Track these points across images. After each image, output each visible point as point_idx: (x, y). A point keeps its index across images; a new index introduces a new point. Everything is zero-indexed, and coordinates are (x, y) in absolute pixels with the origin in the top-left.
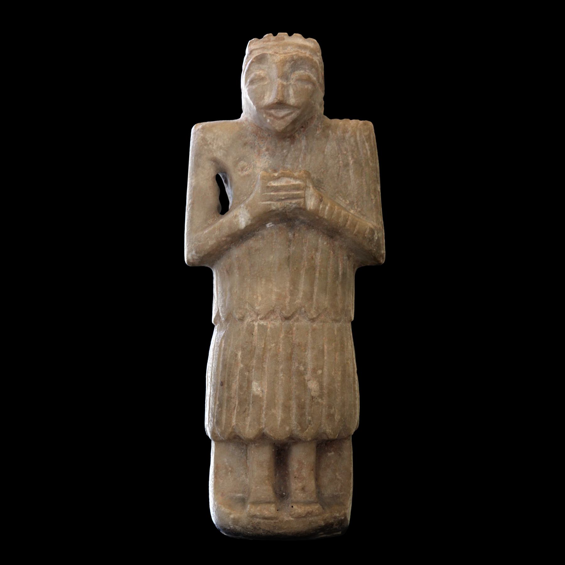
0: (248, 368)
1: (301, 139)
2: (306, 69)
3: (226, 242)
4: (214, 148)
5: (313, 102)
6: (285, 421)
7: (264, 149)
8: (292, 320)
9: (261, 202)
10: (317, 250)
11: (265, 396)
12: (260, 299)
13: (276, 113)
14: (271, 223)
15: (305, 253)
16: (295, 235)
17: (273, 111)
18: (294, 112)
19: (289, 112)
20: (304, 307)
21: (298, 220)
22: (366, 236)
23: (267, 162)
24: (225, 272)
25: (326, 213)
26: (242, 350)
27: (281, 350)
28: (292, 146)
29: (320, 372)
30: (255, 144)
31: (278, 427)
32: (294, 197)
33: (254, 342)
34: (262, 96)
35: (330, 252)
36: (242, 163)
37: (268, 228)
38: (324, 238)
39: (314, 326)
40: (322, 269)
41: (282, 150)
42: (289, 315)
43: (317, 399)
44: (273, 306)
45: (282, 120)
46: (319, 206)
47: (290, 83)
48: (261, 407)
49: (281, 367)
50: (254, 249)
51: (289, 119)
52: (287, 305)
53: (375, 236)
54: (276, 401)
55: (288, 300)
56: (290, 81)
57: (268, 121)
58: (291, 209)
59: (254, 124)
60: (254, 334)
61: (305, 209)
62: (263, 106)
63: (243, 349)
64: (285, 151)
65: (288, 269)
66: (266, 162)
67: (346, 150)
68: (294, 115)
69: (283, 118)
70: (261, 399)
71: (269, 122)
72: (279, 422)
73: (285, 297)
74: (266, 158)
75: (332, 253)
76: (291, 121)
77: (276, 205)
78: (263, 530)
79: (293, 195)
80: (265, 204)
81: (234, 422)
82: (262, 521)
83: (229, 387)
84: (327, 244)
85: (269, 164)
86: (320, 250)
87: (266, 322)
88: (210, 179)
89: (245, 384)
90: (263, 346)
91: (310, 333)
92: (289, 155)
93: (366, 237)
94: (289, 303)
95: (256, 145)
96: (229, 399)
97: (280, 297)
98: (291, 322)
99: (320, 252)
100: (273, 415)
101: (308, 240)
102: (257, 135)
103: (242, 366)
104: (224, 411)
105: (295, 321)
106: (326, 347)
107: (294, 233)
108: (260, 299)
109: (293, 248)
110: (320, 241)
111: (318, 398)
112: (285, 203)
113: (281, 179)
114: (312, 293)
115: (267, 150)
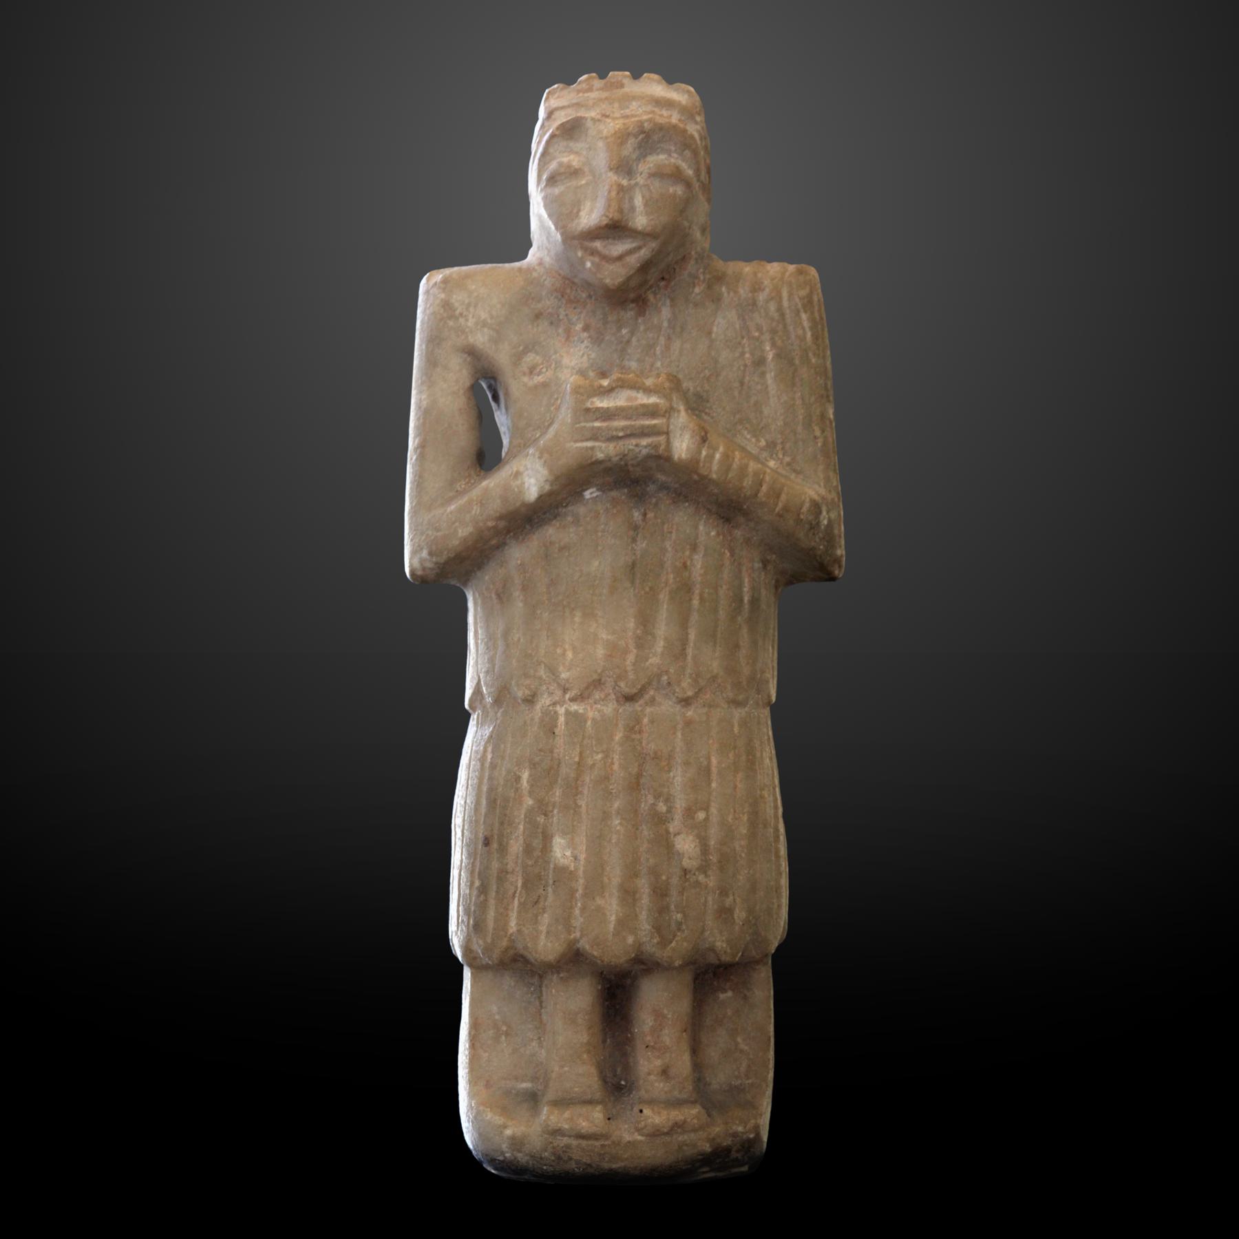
0: (543, 807)
1: (660, 304)
3: (496, 531)
5: (686, 224)
6: (626, 923)
7: (579, 327)
8: (641, 702)
10: (694, 548)
11: (582, 869)
12: (570, 655)
13: (605, 247)
14: (594, 489)
15: (669, 555)
16: (648, 516)
17: (598, 244)
18: (645, 246)
19: (634, 245)
20: (667, 672)
21: (654, 482)
22: (802, 517)
23: (586, 355)
24: (494, 596)
25: (715, 467)
26: (531, 768)
27: (616, 767)
28: (640, 321)
29: (701, 815)
30: (558, 316)
31: (610, 937)
32: (644, 433)
33: (558, 751)
34: (575, 211)
35: (724, 552)
36: (530, 358)
37: (588, 499)
38: (711, 521)
39: (688, 715)
40: (707, 590)
42: (634, 691)
43: (694, 874)
44: (599, 671)
45: (618, 264)
46: (700, 453)
47: (636, 182)
48: (572, 892)
49: (616, 805)
50: (557, 545)
52: (629, 668)
53: (822, 518)
54: (606, 879)
55: (631, 658)
57: (588, 265)
58: (639, 459)
59: (556, 272)
60: (556, 733)
61: (668, 459)
62: (576, 233)
63: (533, 765)
64: (624, 331)
66: (583, 355)
68: (644, 253)
69: (620, 258)
70: (572, 875)
71: (590, 269)
72: (612, 926)
73: (626, 652)
74: (583, 346)
75: (728, 554)
76: (639, 265)
77: (604, 451)
78: (577, 1162)
79: (643, 427)
80: (581, 448)
81: (513, 925)
82: (574, 1142)
83: (503, 850)
84: (718, 534)
85: (589, 359)
86: (701, 549)
87: (583, 707)
88: (462, 392)
89: (537, 843)
91: (681, 731)
93: (802, 520)
94: (634, 664)
95: (561, 317)
96: (503, 874)
97: (614, 651)
98: (637, 706)
99: (703, 552)
100: (599, 909)
102: (563, 296)
104: (492, 902)
105: (646, 704)
106: (714, 761)
107: (645, 510)
108: (570, 655)
109: (642, 545)
110: (701, 528)
111: (697, 873)
112: (624, 445)
113: (617, 393)
114: (684, 642)
115: (586, 328)
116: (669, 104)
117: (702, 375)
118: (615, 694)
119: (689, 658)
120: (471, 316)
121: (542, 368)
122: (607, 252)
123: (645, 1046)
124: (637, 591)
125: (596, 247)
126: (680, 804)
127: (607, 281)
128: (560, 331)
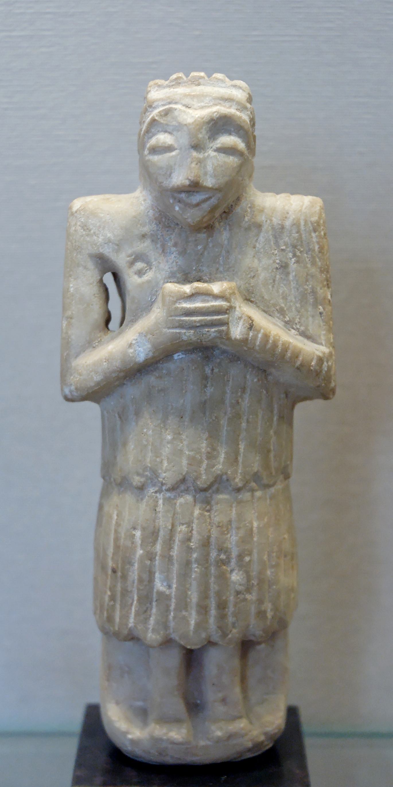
0: (151, 557)
1: (222, 229)
2: (231, 130)
3: (118, 378)
4: (100, 240)
5: (240, 178)
6: (200, 625)
7: (170, 244)
8: (210, 491)
9: (166, 329)
10: (244, 390)
11: (174, 593)
12: (165, 464)
13: (188, 197)
14: (181, 353)
15: (228, 396)
16: (214, 371)
17: (183, 195)
18: (214, 196)
19: (207, 196)
20: (226, 474)
21: (218, 349)
22: (312, 368)
23: (175, 262)
24: (117, 415)
25: (258, 343)
26: (141, 531)
27: (194, 532)
28: (209, 240)
29: (247, 559)
30: (157, 236)
31: (191, 633)
32: (212, 324)
33: (158, 521)
34: (168, 173)
35: (262, 391)
36: (139, 265)
37: (176, 360)
38: (254, 372)
39: (239, 497)
40: (251, 416)
41: (197, 245)
42: (205, 486)
43: (243, 594)
44: (184, 474)
45: (197, 208)
46: (249, 334)
47: (209, 154)
48: (168, 606)
49: (195, 555)
50: (157, 389)
51: (206, 206)
52: (203, 472)
53: (324, 366)
54: (189, 600)
55: (204, 465)
56: (208, 152)
57: (177, 208)
58: (209, 339)
59: (156, 206)
60: (157, 510)
61: (229, 339)
62: (169, 188)
63: (144, 529)
64: (199, 247)
65: (204, 419)
66: (173, 262)
67: (286, 244)
68: (213, 201)
69: (198, 205)
70: (168, 598)
71: (178, 211)
72: (192, 627)
73: (200, 462)
74: (173, 256)
75: (265, 392)
76: (210, 209)
77: (188, 335)
78: (172, 757)
79: (212, 321)
80: (173, 333)
81: (131, 622)
82: (170, 746)
83: (124, 577)
84: (259, 380)
85: (177, 265)
86: (248, 391)
87: (174, 494)
88: (95, 283)
89: (145, 576)
90: (170, 527)
91: (235, 508)
92: (206, 253)
93: (312, 370)
94: (205, 470)
95: (159, 237)
96: (125, 592)
97: (194, 462)
98: (208, 494)
99: (249, 392)
100: (184, 618)
101: (231, 377)
102: (160, 223)
103: (141, 552)
104: (118, 606)
105: (213, 492)
106: (255, 524)
107: (213, 367)
108: (165, 464)
109: (210, 390)
110: (248, 377)
111: (245, 593)
112: (200, 332)
113: (196, 297)
114: (237, 453)
115: (175, 245)
116: (229, 100)
117: (249, 276)
118: (194, 487)
119: (240, 464)
120: (101, 235)
121: (147, 270)
122: (189, 202)
123: (184, 369)
124: (207, 419)
125: (182, 197)
126: (234, 553)
127: (189, 220)
128: (159, 246)
